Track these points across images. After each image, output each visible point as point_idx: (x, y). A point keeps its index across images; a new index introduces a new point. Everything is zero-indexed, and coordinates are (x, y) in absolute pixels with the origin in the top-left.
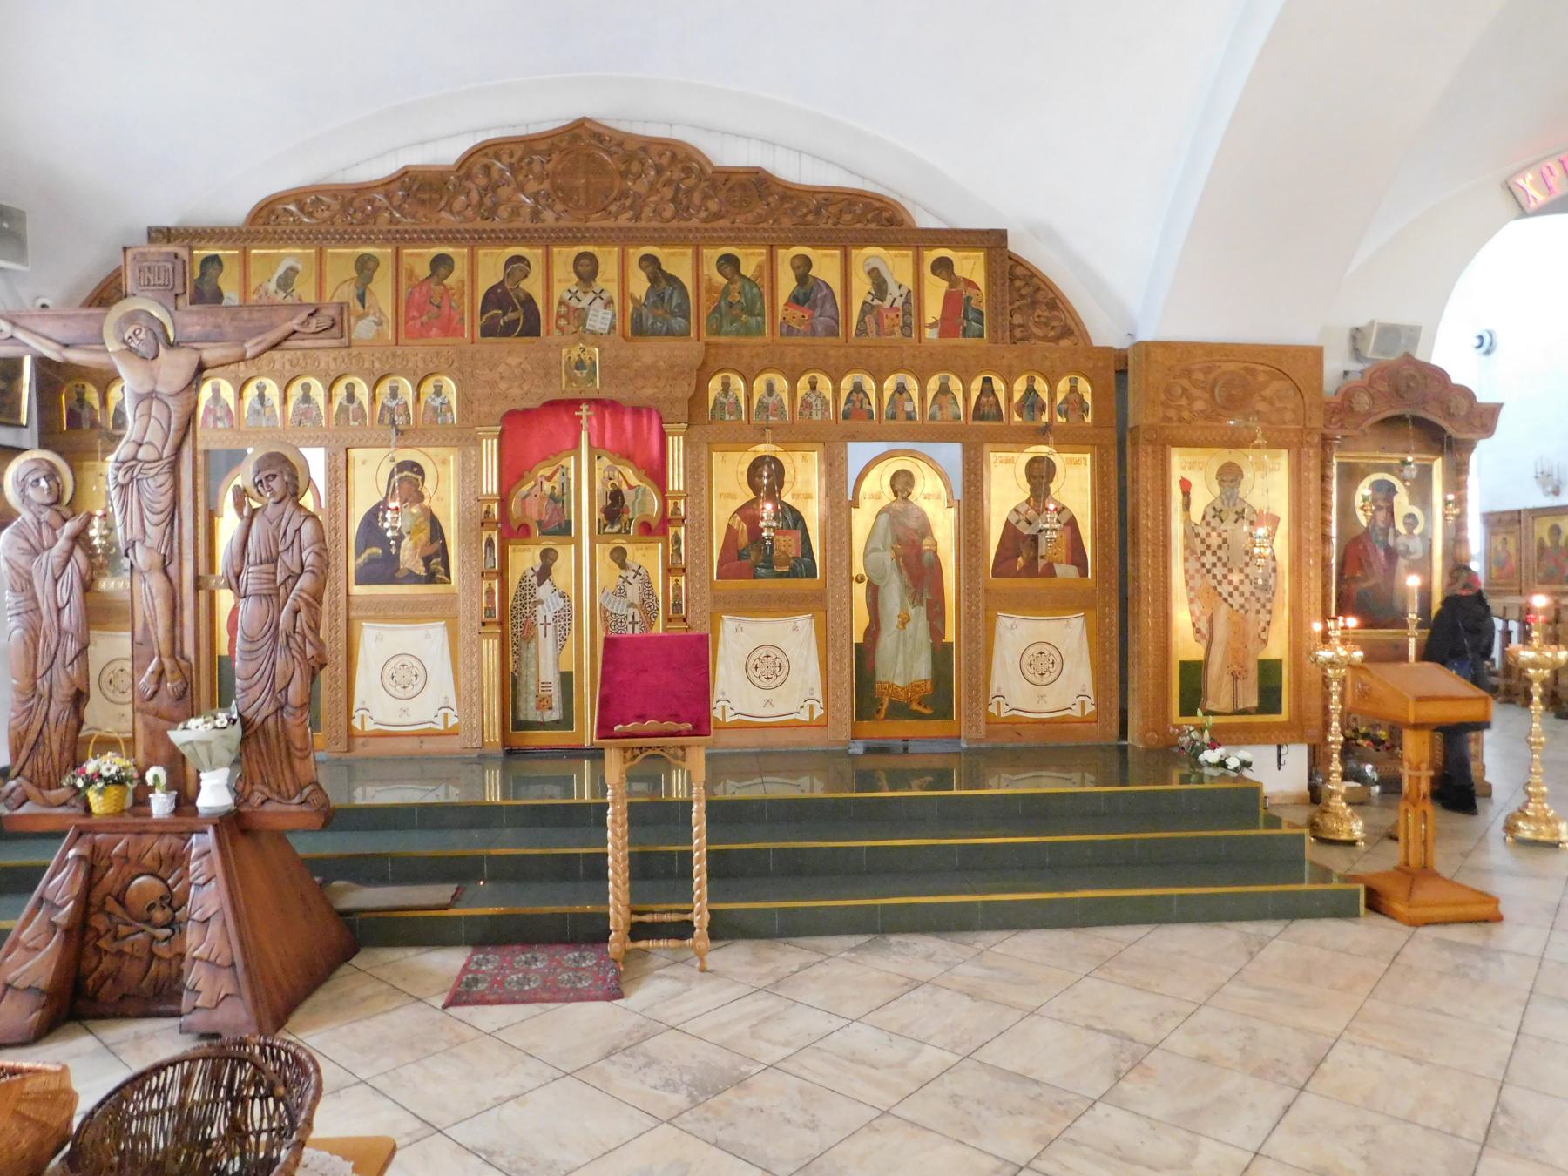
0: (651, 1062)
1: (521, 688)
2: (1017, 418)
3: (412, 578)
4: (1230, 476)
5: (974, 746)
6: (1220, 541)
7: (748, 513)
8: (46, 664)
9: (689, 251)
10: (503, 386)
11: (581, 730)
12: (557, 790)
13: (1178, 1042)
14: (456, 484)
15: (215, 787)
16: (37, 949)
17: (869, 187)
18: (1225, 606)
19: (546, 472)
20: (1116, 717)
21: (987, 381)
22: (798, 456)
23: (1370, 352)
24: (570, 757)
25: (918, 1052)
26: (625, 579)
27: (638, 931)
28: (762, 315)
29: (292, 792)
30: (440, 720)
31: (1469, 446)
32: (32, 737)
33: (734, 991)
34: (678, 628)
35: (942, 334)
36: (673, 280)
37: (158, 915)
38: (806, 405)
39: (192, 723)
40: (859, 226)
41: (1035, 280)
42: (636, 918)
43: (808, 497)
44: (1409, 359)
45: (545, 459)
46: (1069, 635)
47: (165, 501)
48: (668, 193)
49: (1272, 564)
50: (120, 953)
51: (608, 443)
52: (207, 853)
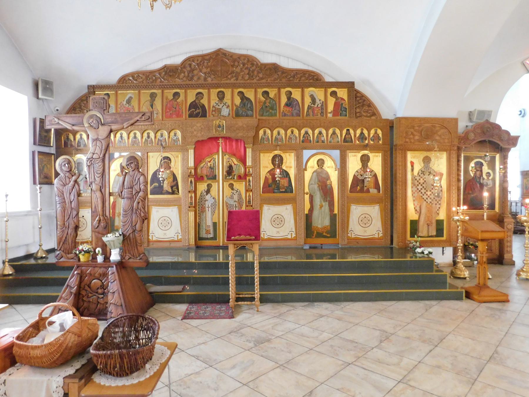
0: (243, 335)
1: (201, 227)
2: (357, 142)
3: (168, 193)
4: (427, 160)
5: (344, 246)
6: (423, 181)
7: (272, 172)
8: (67, 217)
9: (253, 90)
10: (195, 133)
11: (219, 240)
12: (212, 259)
13: (401, 333)
14: (181, 163)
15: (115, 254)
16: (67, 299)
17: (310, 69)
18: (425, 202)
19: (209, 160)
20: (389, 237)
21: (348, 130)
22: (288, 154)
23: (475, 119)
24: (216, 249)
25: (321, 334)
26: (233, 193)
27: (238, 299)
28: (276, 110)
29: (137, 255)
30: (176, 237)
31: (508, 150)
32: (64, 238)
33: (266, 317)
34: (250, 208)
35: (333, 116)
36: (248, 99)
37: (100, 291)
38: (290, 138)
39: (109, 235)
40: (307, 81)
41: (363, 98)
42: (237, 296)
43: (291, 167)
44: (487, 122)
45: (208, 155)
46: (374, 212)
47: (101, 170)
48: (246, 71)
49: (441, 189)
50: (89, 302)
51: (228, 150)
52: (113, 273)
